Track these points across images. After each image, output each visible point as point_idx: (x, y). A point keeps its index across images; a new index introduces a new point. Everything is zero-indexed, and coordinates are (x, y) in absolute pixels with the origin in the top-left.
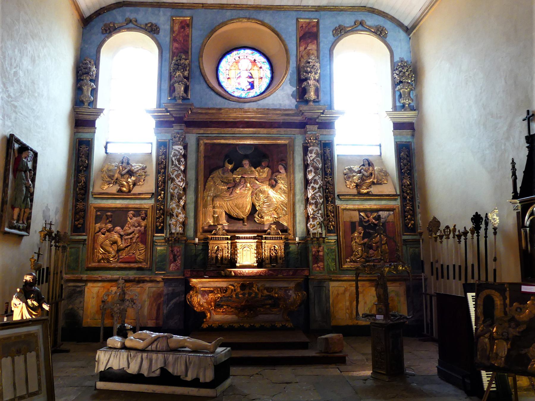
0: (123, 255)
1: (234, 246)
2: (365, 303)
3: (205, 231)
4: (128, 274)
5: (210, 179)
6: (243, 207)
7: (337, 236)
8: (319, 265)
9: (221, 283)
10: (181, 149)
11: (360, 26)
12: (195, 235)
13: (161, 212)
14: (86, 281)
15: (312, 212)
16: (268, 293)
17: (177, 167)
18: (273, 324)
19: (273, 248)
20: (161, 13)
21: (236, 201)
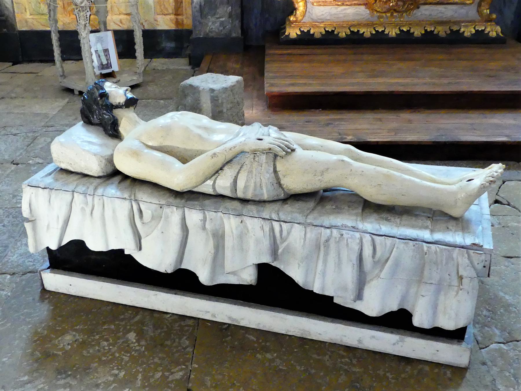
18: (455, 28)
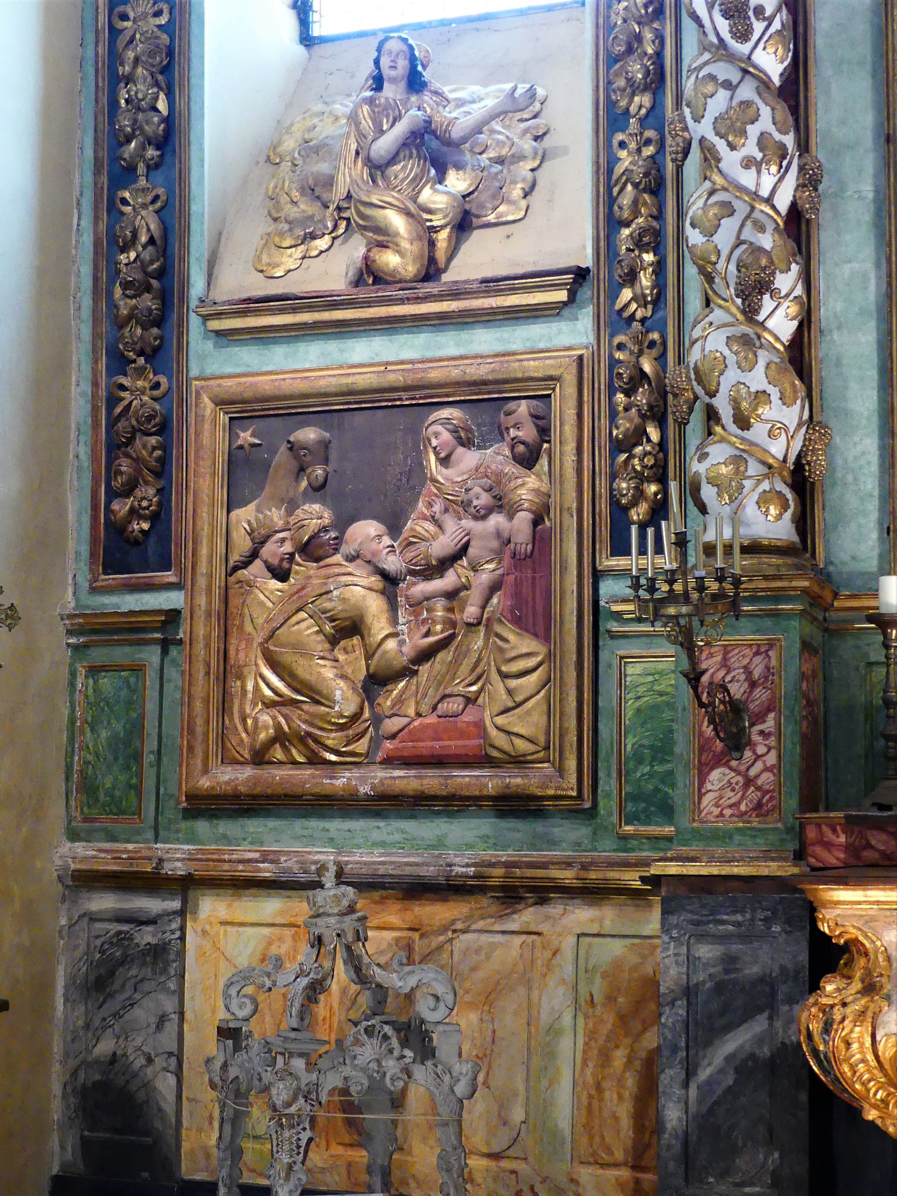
0: (406, 708)
4: (440, 843)
13: (642, 397)
14: (187, 886)
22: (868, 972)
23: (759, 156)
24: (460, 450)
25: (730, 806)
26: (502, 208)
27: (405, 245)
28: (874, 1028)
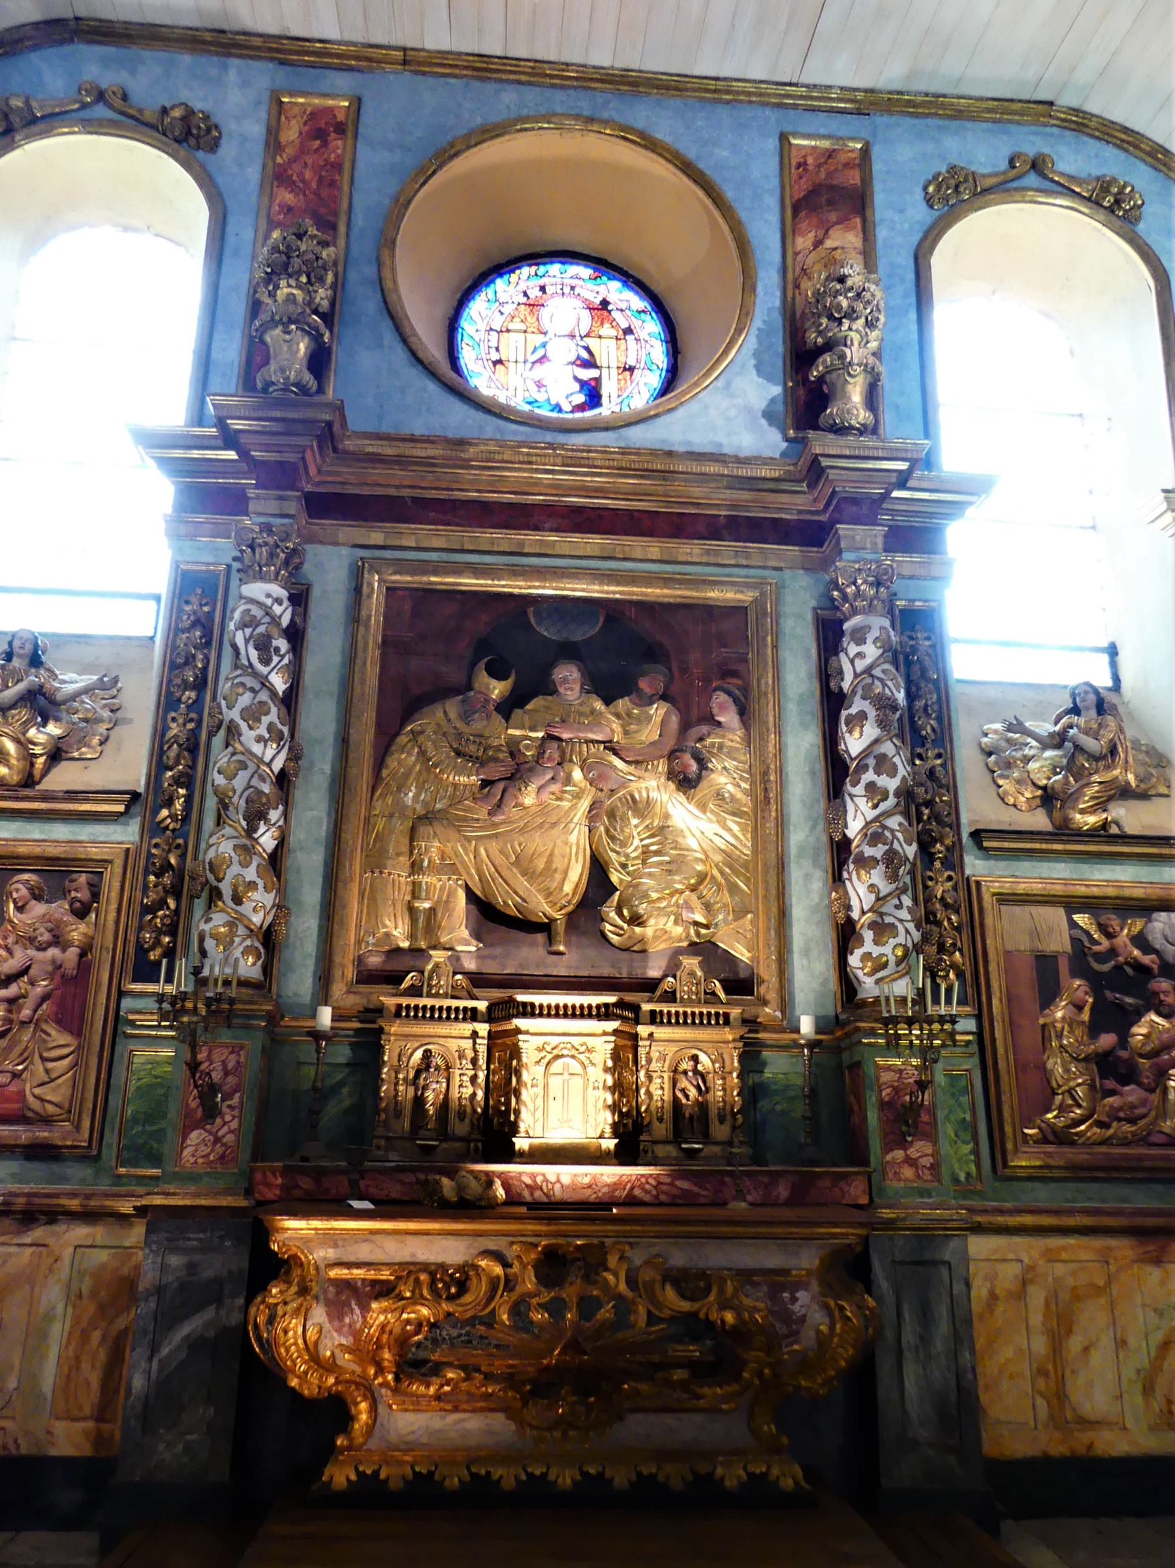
1: (504, 1054)
2: (1121, 1344)
3: (368, 977)
5: (403, 739)
6: (549, 870)
7: (979, 1017)
8: (913, 1152)
9: (437, 1244)
10: (279, 601)
11: (1029, 176)
12: (323, 994)
13: (167, 880)
15: (869, 900)
16: (686, 1306)
17: (255, 674)
18: (703, 1468)
19: (686, 1065)
20: (232, 75)
21: (518, 838)
22: (303, 1278)
23: (267, 736)
24: (33, 902)
25: (203, 1157)
26: (84, 750)
27: (14, 762)
28: (305, 1320)
